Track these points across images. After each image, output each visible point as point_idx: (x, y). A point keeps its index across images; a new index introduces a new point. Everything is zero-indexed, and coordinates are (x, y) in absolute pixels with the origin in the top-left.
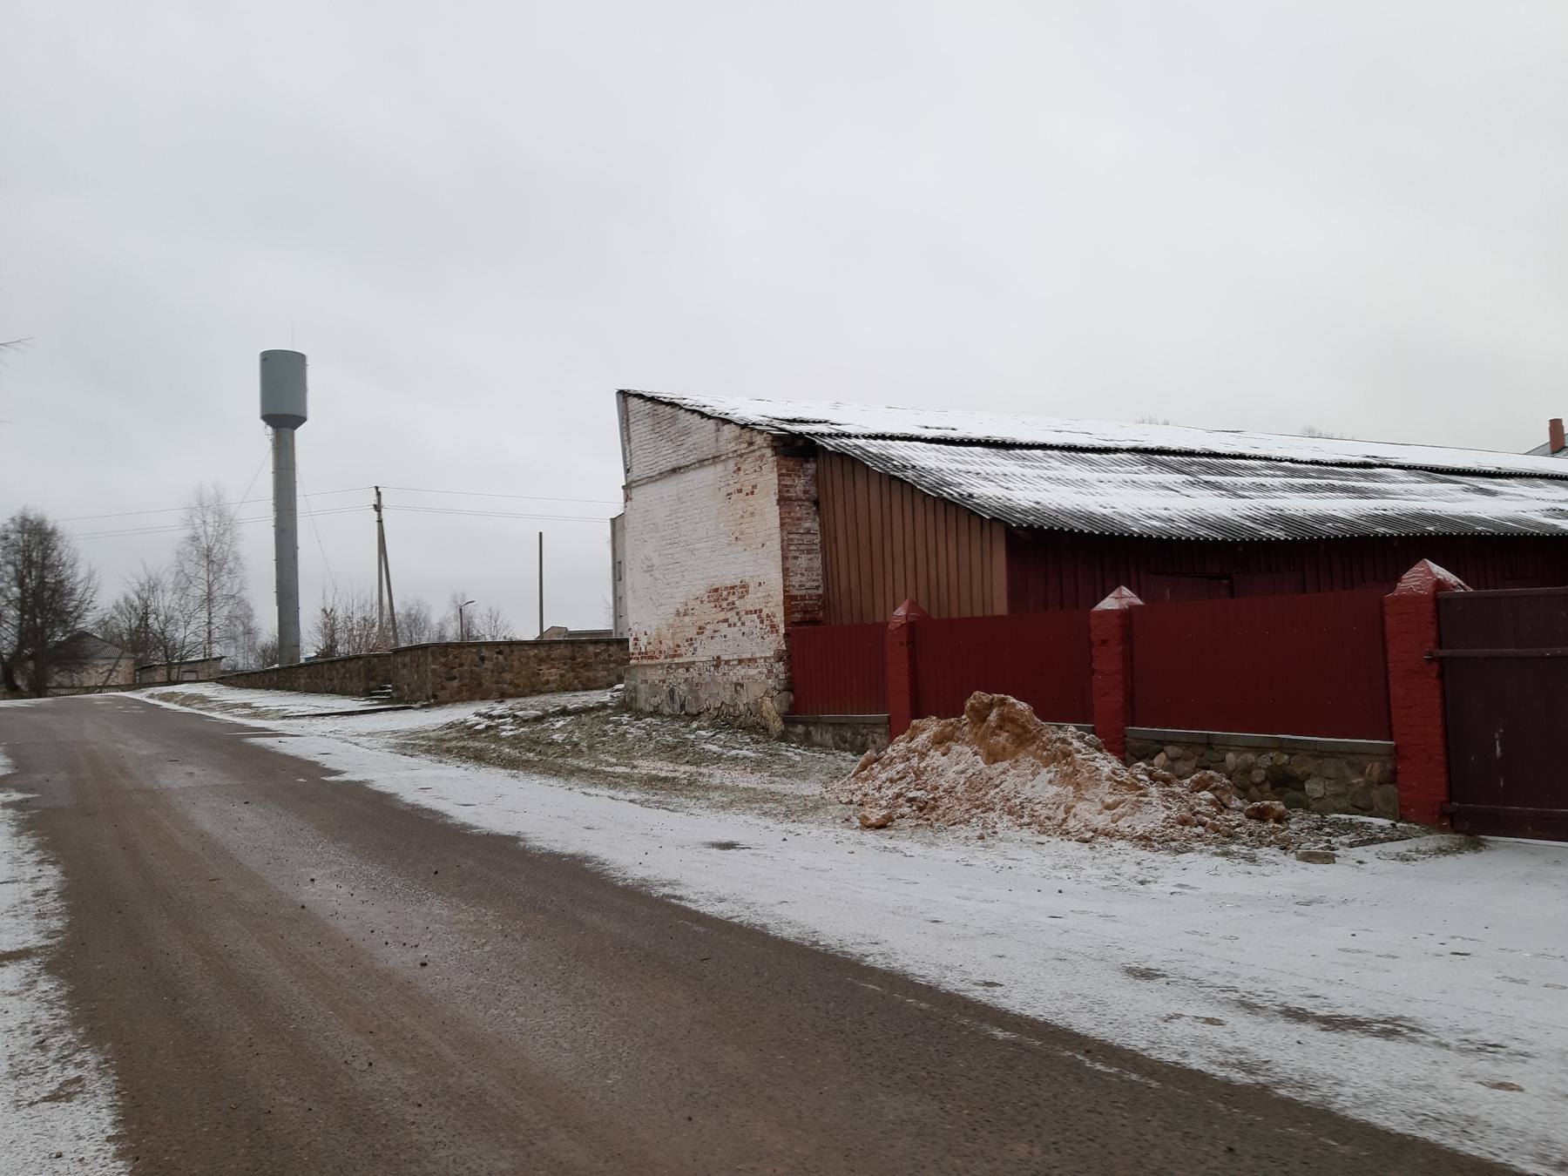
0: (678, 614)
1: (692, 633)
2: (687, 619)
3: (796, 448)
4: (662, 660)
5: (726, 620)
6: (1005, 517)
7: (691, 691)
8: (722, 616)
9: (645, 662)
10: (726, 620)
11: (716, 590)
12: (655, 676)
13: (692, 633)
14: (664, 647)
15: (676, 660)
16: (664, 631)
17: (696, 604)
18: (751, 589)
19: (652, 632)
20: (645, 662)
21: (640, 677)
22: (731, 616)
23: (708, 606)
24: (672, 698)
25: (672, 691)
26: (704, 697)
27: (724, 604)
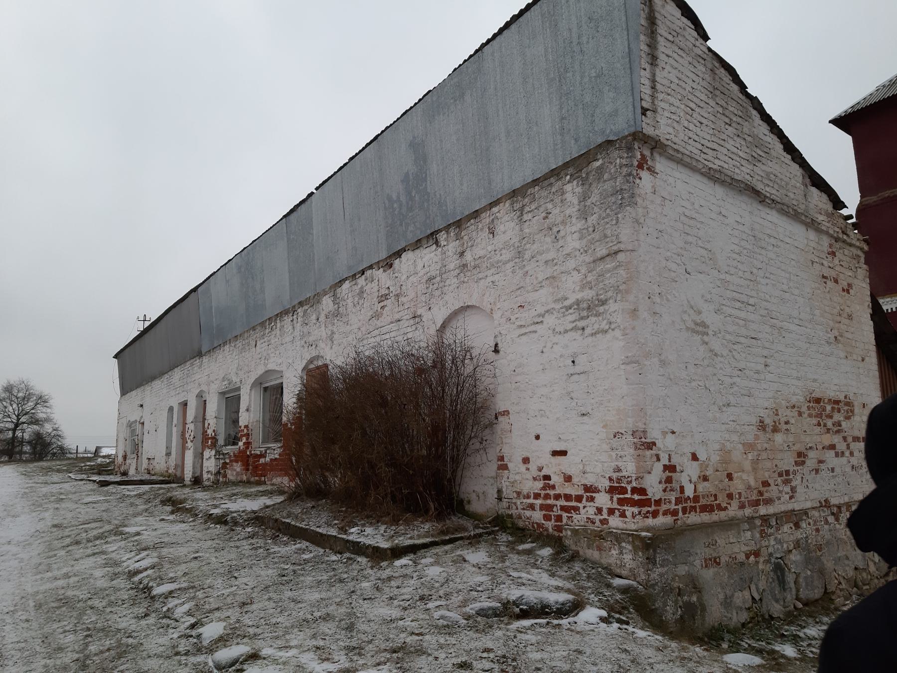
0: (762, 426)
1: (787, 462)
2: (779, 438)
3: (126, 388)
4: (733, 510)
5: (832, 447)
6: (372, 377)
7: (808, 561)
8: (827, 439)
9: (694, 518)
10: (832, 447)
11: (818, 401)
12: (735, 545)
13: (787, 462)
14: (737, 486)
15: (763, 510)
16: (737, 455)
17: (792, 414)
18: (856, 411)
19: (709, 454)
20: (694, 518)
21: (701, 551)
22: (836, 439)
23: (809, 422)
24: (782, 582)
25: (779, 569)
26: (829, 565)
27: (829, 423)
